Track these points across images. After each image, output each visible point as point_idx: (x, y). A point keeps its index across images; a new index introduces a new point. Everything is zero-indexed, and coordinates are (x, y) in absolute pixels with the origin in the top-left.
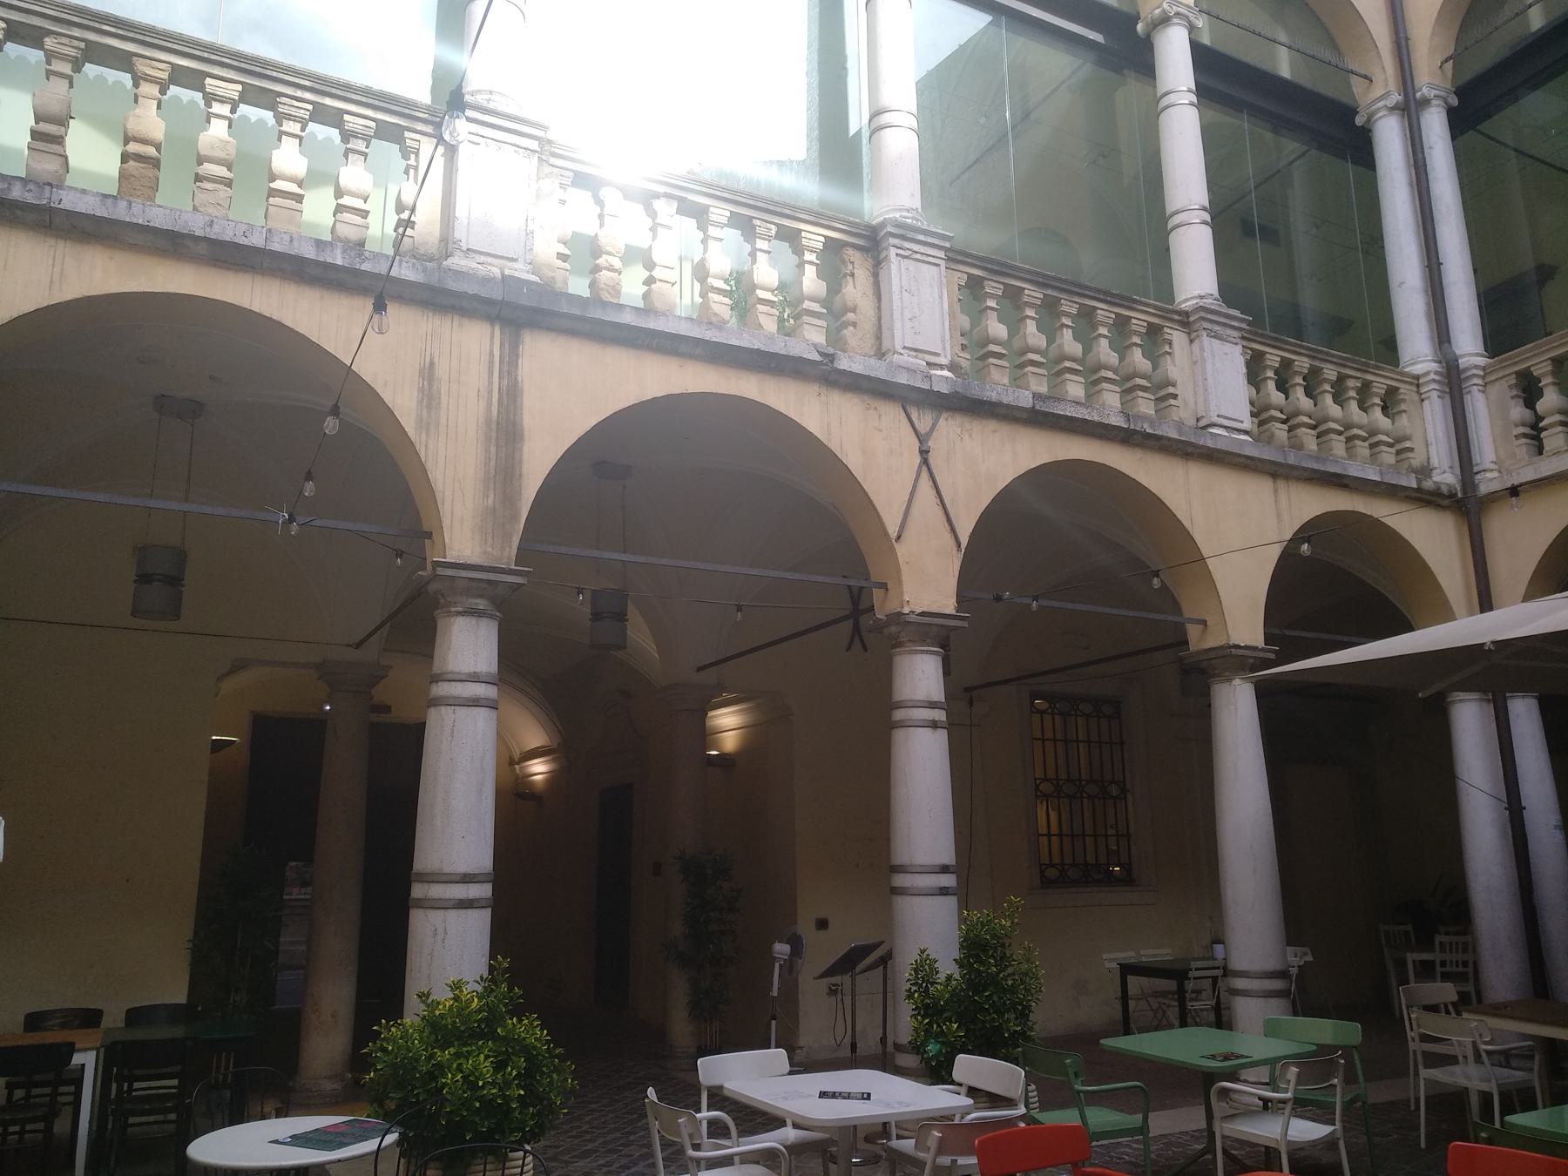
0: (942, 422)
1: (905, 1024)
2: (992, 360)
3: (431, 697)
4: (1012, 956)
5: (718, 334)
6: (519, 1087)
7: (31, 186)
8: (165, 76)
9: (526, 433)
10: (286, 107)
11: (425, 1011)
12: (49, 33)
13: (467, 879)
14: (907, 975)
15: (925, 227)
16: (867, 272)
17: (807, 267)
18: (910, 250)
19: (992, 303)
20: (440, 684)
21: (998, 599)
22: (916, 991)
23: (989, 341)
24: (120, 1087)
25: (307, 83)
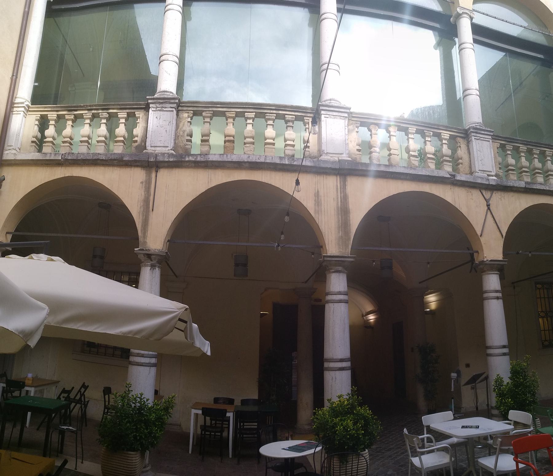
0: (494, 194)
1: (494, 400)
2: (510, 172)
3: (326, 300)
4: (528, 375)
5: (414, 171)
6: (362, 430)
7: (202, 156)
8: (234, 115)
9: (351, 211)
10: (268, 116)
11: (330, 405)
12: (204, 111)
13: (342, 360)
14: (493, 383)
15: (484, 129)
16: (465, 145)
17: (444, 145)
18: (479, 137)
19: (509, 152)
20: (328, 296)
21: (518, 253)
22: (496, 389)
23: (508, 165)
24: (240, 424)
25: (274, 108)
